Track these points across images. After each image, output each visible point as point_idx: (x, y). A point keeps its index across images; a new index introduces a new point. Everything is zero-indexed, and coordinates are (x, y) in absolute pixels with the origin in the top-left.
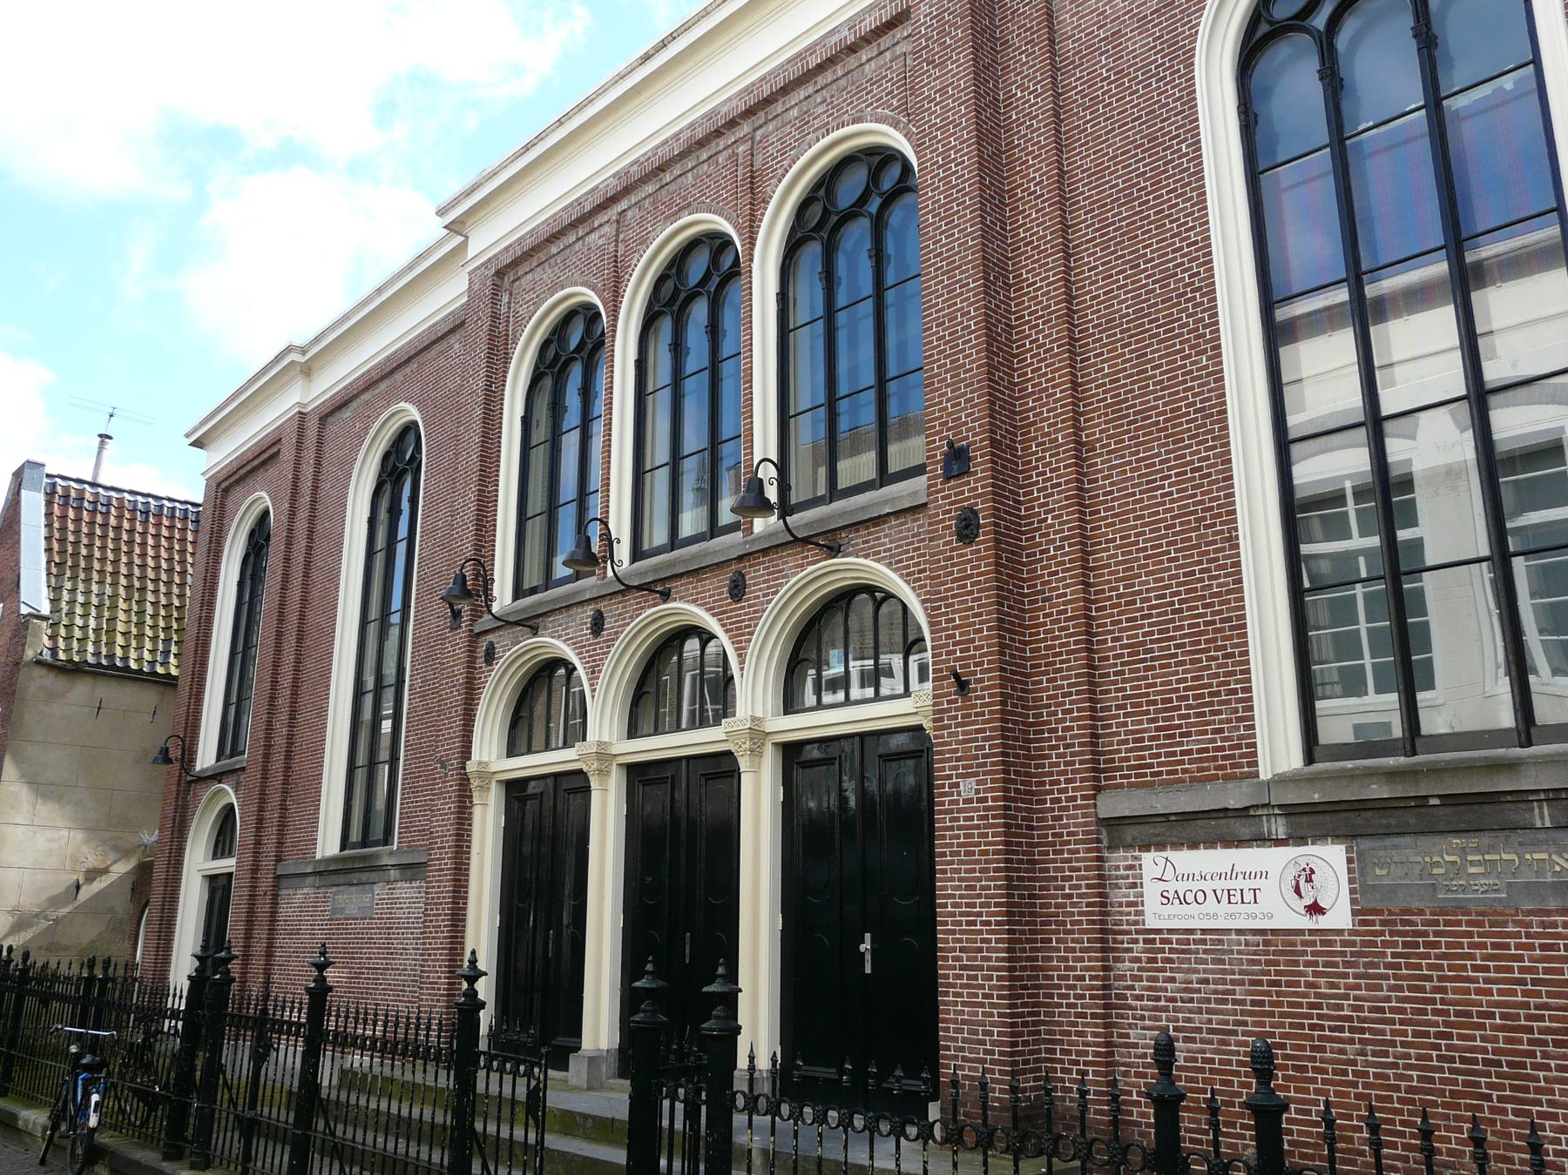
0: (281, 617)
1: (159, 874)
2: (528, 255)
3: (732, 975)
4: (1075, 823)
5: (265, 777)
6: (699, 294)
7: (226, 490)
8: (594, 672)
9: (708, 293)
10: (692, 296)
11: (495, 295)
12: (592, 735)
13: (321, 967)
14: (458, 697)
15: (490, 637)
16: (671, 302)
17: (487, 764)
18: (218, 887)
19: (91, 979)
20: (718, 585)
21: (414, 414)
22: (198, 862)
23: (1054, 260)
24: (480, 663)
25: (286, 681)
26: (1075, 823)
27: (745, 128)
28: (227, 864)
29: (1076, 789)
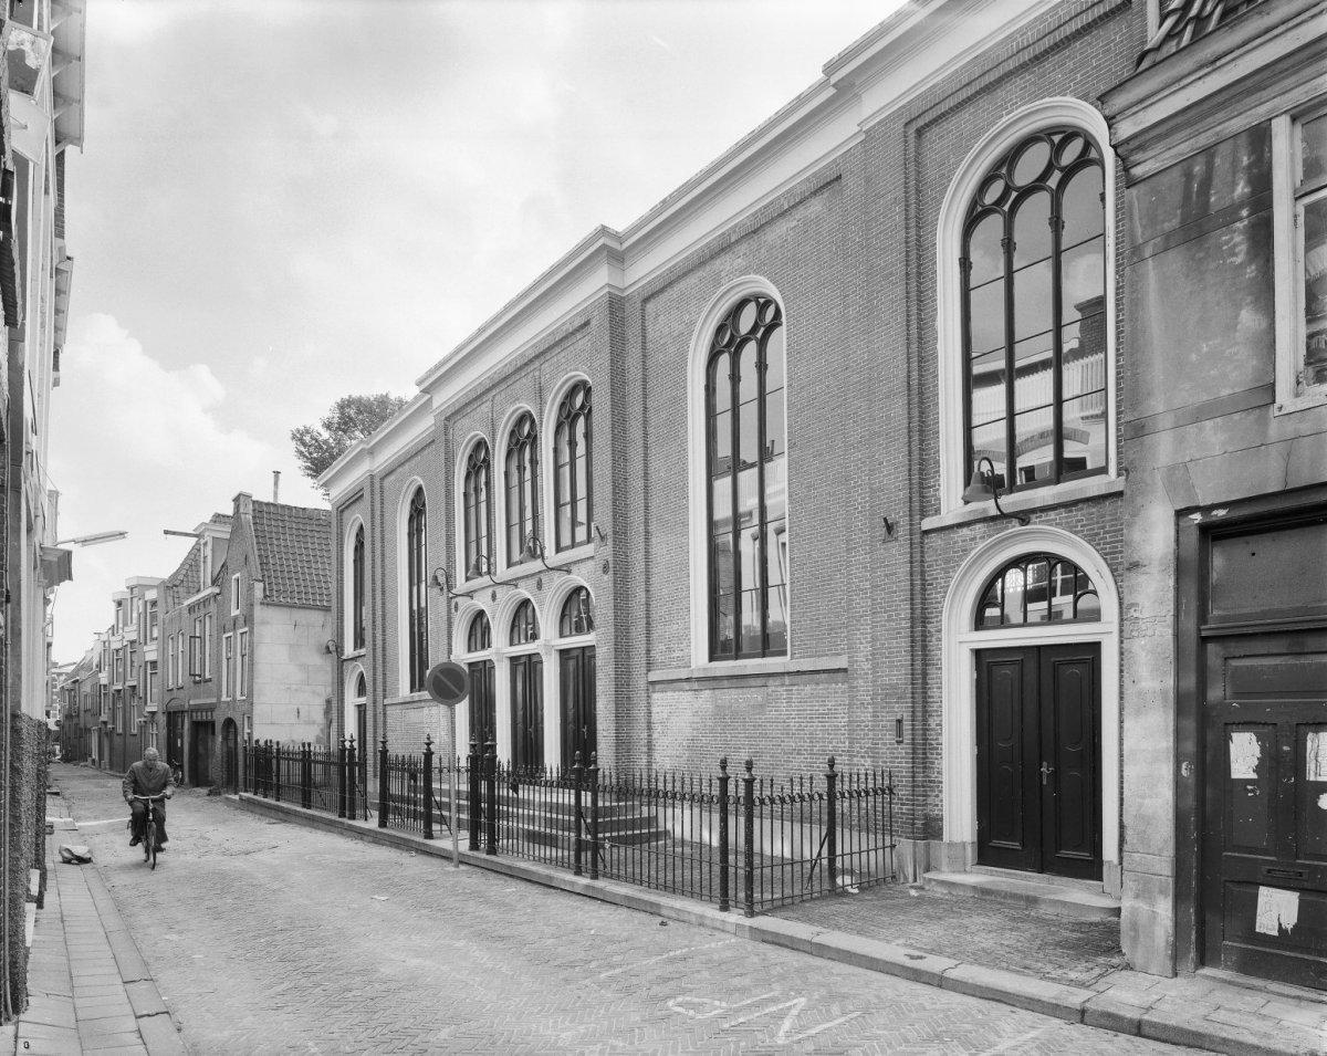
0: (373, 580)
1: (334, 704)
2: (457, 412)
3: (494, 739)
4: (642, 684)
5: (374, 660)
6: (750, 339)
7: (342, 511)
8: (541, 604)
9: (756, 339)
10: (745, 340)
11: (446, 428)
12: (494, 645)
13: (428, 744)
14: (444, 626)
15: (457, 599)
16: (728, 345)
17: (548, 641)
18: (361, 709)
19: (304, 752)
20: (533, 582)
21: (421, 482)
22: (351, 699)
23: (641, 450)
24: (453, 611)
25: (379, 613)
26: (642, 684)
27: (537, 364)
28: (362, 700)
29: (644, 670)
